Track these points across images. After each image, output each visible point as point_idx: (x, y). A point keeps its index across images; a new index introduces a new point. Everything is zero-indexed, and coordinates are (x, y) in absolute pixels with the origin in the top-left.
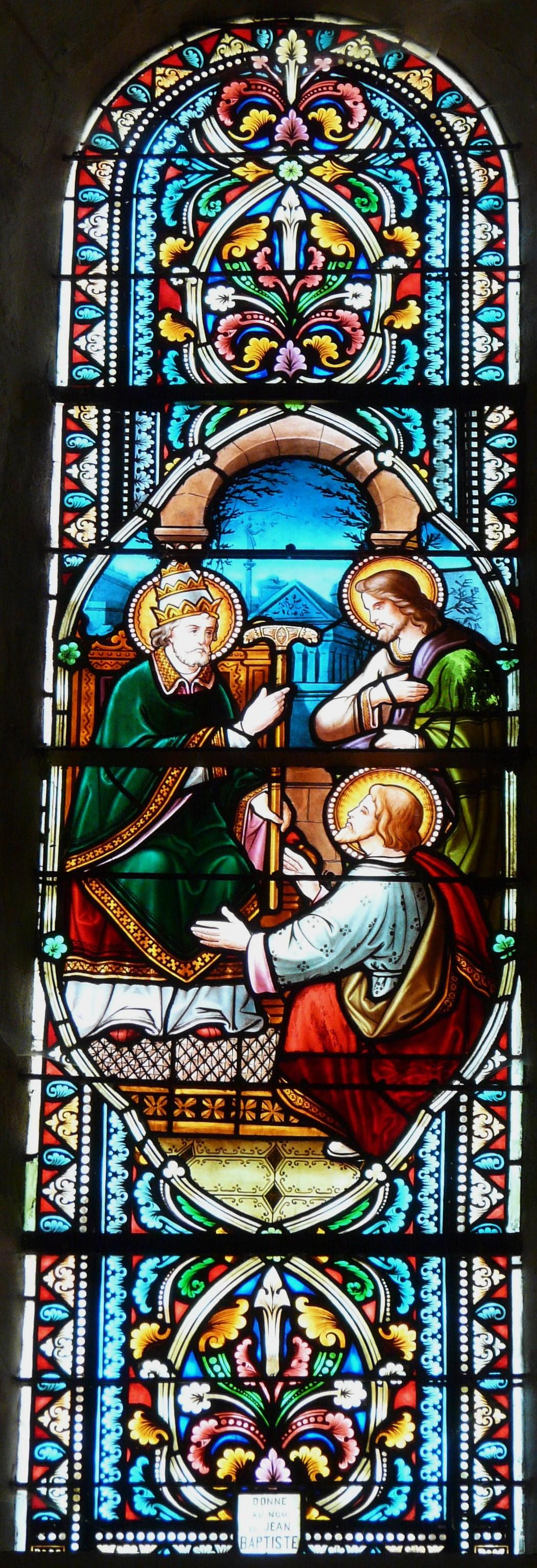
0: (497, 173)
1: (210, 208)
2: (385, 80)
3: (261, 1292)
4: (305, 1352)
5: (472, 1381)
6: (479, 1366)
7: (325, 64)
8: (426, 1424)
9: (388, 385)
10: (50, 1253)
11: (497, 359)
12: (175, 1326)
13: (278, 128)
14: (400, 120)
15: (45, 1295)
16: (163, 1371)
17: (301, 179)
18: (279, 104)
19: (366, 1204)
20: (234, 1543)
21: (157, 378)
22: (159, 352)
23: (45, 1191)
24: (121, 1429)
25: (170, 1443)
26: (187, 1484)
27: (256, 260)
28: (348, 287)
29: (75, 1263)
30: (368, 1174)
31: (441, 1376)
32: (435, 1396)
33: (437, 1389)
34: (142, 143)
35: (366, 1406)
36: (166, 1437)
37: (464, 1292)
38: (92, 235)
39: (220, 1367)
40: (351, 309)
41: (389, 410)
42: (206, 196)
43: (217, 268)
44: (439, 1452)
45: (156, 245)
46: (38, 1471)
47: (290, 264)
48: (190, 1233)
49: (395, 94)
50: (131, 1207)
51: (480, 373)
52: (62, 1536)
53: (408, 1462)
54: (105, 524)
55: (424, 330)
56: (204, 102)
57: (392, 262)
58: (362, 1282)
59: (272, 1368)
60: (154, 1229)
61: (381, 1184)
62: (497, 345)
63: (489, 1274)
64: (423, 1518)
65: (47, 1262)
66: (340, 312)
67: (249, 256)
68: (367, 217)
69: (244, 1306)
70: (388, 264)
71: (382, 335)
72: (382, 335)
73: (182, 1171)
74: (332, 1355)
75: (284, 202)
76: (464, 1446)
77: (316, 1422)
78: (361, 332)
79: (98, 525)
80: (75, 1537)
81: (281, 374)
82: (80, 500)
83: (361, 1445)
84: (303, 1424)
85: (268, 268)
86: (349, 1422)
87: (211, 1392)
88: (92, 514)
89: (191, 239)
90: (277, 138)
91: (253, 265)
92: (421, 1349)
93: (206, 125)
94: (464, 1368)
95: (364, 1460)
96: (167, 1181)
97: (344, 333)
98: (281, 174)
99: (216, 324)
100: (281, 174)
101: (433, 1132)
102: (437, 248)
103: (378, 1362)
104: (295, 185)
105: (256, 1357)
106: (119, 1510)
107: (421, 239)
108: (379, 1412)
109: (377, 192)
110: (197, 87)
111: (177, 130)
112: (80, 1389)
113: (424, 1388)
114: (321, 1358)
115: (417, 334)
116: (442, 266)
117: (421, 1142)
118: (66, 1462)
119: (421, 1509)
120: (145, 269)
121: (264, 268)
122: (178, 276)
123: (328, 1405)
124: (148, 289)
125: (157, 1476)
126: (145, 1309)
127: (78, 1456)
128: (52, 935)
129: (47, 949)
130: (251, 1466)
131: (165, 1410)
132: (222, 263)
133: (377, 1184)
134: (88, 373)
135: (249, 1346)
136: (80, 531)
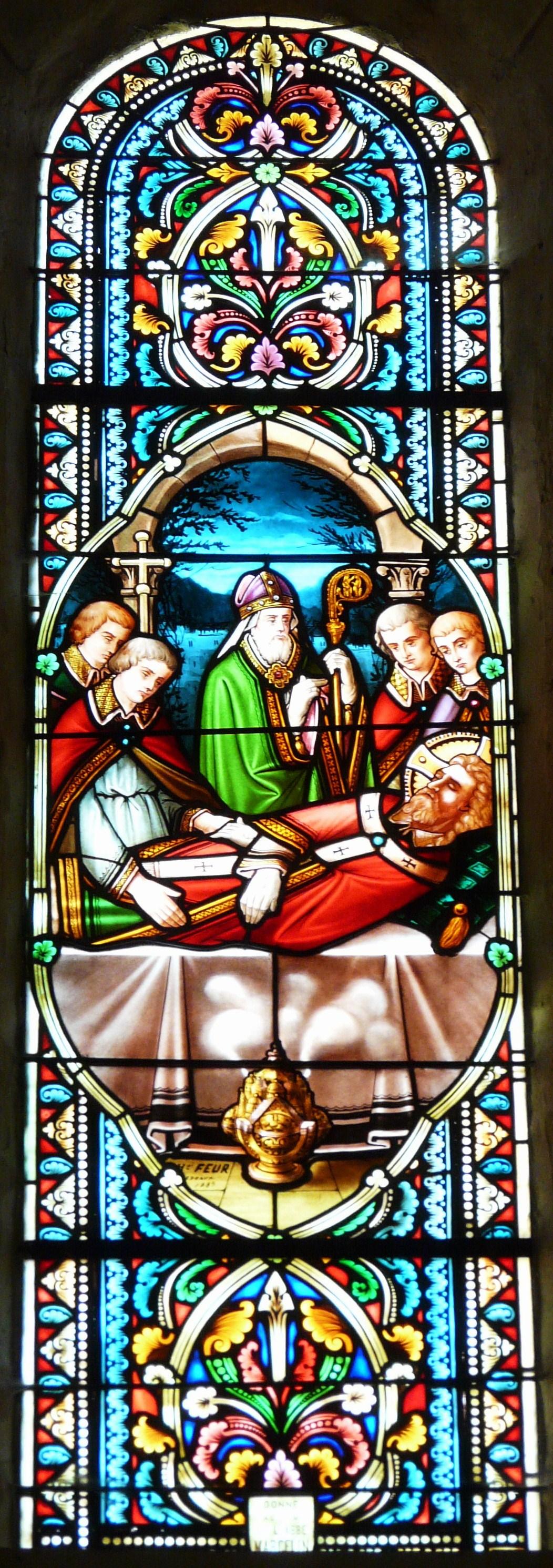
0: (475, 177)
1: (190, 1290)
3: (257, 210)
4: (310, 1355)
9: (370, 390)
11: (480, 363)
12: (178, 1329)
17: (279, 181)
19: (370, 1210)
23: (44, 1202)
24: (128, 250)
25: (176, 1450)
26: (195, 1489)
27: (232, 260)
30: (369, 1181)
31: (424, 272)
32: (445, 1396)
33: (420, 284)
34: (113, 146)
35: (375, 1411)
36: (172, 1443)
39: (226, 1370)
40: (349, 1415)
41: (384, 1262)
43: (193, 266)
46: (43, 1476)
47: (268, 265)
48: (187, 386)
49: (371, 98)
53: (420, 1466)
54: (85, 525)
56: (177, 105)
57: (371, 266)
58: (364, 1281)
59: (279, 1373)
61: (384, 1190)
62: (479, 349)
67: (227, 254)
69: (241, 220)
73: (179, 1180)
74: (339, 1360)
75: (262, 201)
76: (476, 1450)
77: (324, 1426)
78: (344, 338)
79: (79, 528)
81: (261, 374)
85: (246, 269)
87: (217, 1397)
88: (72, 516)
89: (169, 231)
90: (253, 142)
91: (230, 265)
92: (428, 1349)
93: (179, 127)
96: (165, 1190)
97: (320, 108)
98: (258, 178)
99: (197, 1434)
100: (258, 178)
101: (437, 1133)
104: (272, 186)
106: (127, 1513)
108: (389, 1416)
109: (375, 1277)
110: (170, 92)
112: (83, 1494)
113: (433, 1390)
114: (328, 1362)
115: (400, 340)
116: (451, 1486)
117: (426, 1145)
118: (79, 319)
121: (241, 268)
122: (155, 271)
123: (336, 1410)
124: (124, 309)
126: (146, 1313)
128: (45, 651)
129: (39, 666)
131: (171, 1417)
132: (199, 259)
133: (379, 1190)
134: (63, 370)
135: (244, 254)
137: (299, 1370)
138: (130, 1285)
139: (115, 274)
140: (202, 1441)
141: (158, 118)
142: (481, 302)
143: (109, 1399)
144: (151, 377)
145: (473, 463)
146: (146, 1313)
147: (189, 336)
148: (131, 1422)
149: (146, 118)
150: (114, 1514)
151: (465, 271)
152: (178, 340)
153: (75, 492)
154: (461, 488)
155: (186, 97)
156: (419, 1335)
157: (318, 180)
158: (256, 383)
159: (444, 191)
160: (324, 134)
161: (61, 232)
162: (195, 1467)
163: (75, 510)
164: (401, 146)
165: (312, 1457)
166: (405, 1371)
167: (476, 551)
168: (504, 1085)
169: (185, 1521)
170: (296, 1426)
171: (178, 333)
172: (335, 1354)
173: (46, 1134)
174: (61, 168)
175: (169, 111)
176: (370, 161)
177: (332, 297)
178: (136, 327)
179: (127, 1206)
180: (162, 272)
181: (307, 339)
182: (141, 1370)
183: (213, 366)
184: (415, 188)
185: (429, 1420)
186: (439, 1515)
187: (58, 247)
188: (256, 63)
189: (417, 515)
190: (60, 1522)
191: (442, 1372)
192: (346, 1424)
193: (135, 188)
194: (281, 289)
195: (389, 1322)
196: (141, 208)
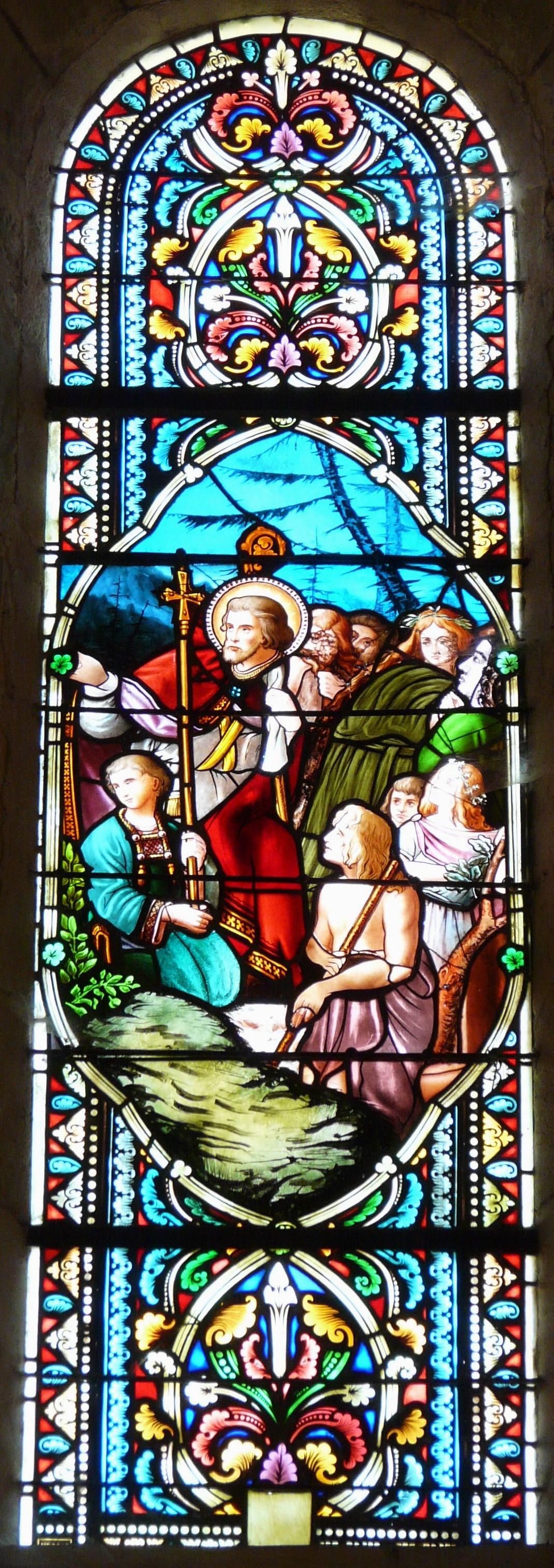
3: (274, 216)
4: (313, 1349)
11: (496, 368)
14: (392, 132)
15: (47, 1356)
18: (273, 114)
20: (243, 1537)
26: (199, 1486)
27: (251, 266)
28: (341, 292)
35: (368, 311)
37: (476, 1429)
40: (345, 314)
42: (200, 206)
45: (130, 1322)
50: (137, 1205)
51: (478, 267)
52: (70, 1529)
53: (419, 1459)
55: (421, 261)
58: (361, 206)
60: (154, 1510)
61: (392, 1176)
63: (501, 1411)
66: (335, 319)
67: (246, 260)
68: (364, 227)
69: (259, 225)
70: (383, 274)
71: (380, 341)
72: (380, 341)
80: (82, 1529)
81: (276, 371)
82: (81, 322)
86: (352, 323)
89: (186, 240)
91: (249, 271)
93: (196, 135)
99: (198, 1420)
102: (432, 255)
104: (289, 195)
105: (262, 1352)
106: (126, 1504)
107: (417, 247)
109: (379, 1272)
110: (188, 99)
117: (429, 1142)
119: (434, 1508)
122: (173, 278)
123: (333, 310)
125: (165, 1478)
126: (165, 223)
132: (218, 265)
136: (81, 295)
139: (130, 280)
140: (203, 1428)
141: (176, 127)
142: (512, 1151)
143: (112, 1391)
144: (154, 1206)
146: (165, 223)
147: (203, 340)
148: (147, 313)
149: (164, 126)
150: (113, 1503)
151: (484, 280)
152: (193, 345)
153: (96, 257)
155: (203, 105)
156: (412, 243)
158: (269, 381)
159: (461, 204)
161: (75, 304)
162: (208, 128)
165: (312, 344)
168: (499, 434)
169: (183, 1512)
171: (193, 338)
174: (78, 179)
177: (348, 301)
178: (152, 331)
179: (127, 1475)
180: (179, 278)
181: (325, 1448)
183: (227, 368)
189: (434, 522)
190: (58, 1509)
191: (434, 274)
193: (153, 196)
194: (299, 293)
195: (385, 231)
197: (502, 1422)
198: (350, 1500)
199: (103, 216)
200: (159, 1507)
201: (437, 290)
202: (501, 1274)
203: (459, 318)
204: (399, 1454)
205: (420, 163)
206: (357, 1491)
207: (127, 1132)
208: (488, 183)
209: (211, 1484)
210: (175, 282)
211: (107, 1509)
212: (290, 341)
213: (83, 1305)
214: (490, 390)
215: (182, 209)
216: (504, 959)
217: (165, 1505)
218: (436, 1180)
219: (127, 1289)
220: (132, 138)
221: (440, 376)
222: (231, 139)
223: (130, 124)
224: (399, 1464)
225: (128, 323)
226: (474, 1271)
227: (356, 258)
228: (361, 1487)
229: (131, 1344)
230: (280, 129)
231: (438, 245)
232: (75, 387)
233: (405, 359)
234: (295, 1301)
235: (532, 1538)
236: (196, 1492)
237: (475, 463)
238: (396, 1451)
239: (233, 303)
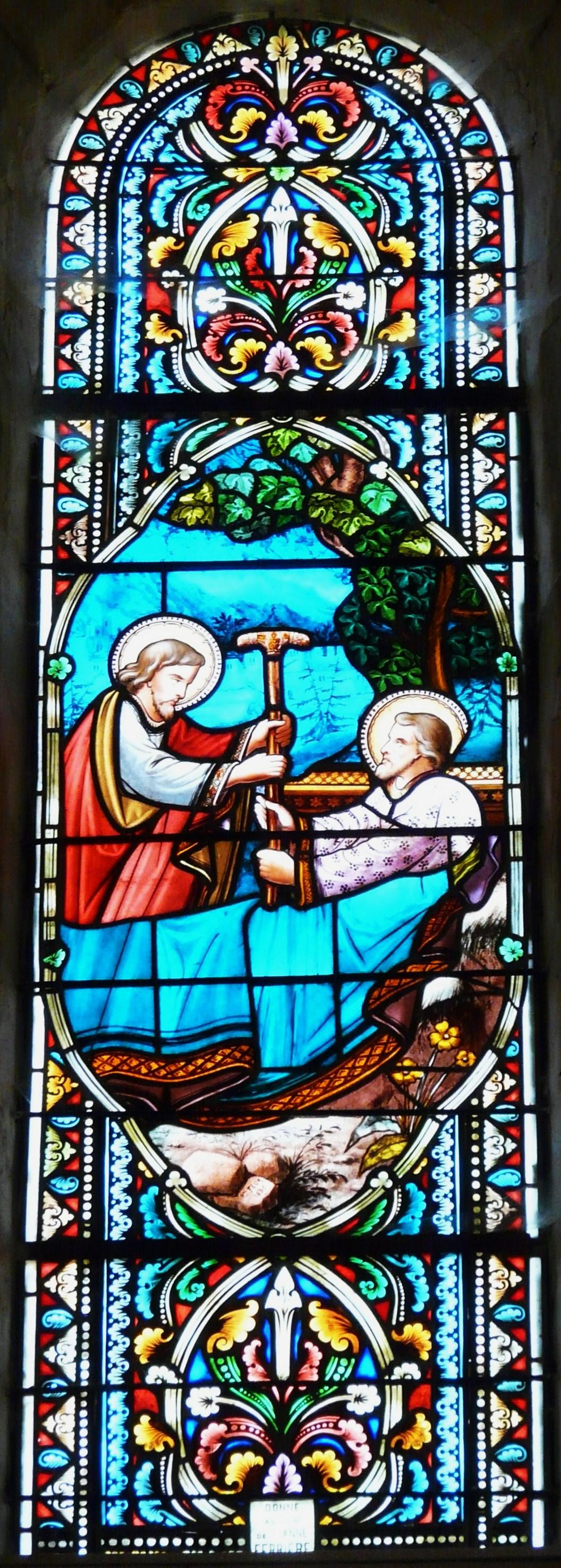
1: (190, 1291)
2: (393, 1543)
3: (270, 210)
5: (489, 1383)
6: (494, 1370)
7: (315, 63)
8: (442, 1424)
10: (50, 1260)
11: (496, 359)
13: (268, 359)
16: (171, 1377)
17: (293, 179)
21: (136, 1231)
22: (135, 1459)
25: (176, 1450)
26: (199, 1497)
29: (78, 1269)
32: (451, 1395)
35: (379, 1412)
36: (171, 1443)
38: (78, 243)
41: (392, 1260)
44: (456, 1452)
45: (143, 248)
56: (192, 102)
59: (283, 1370)
60: (155, 1522)
63: (506, 1276)
64: (440, 1520)
65: (47, 1269)
68: (364, 222)
69: (253, 1306)
70: (398, 1373)
75: (278, 1283)
81: (273, 147)
83: (374, 1451)
84: (316, 1428)
92: (436, 1348)
93: (194, 128)
94: (481, 1370)
95: (378, 1463)
103: (391, 1362)
104: (287, 185)
105: (266, 1359)
108: (394, 1414)
110: (184, 89)
111: (166, 130)
112: (84, 1503)
117: (435, 1141)
119: (438, 1511)
120: (134, 272)
122: (169, 280)
123: (340, 1411)
127: (84, 1462)
130: (262, 355)
131: (172, 1415)
137: (305, 1370)
138: (131, 1288)
141: (172, 116)
145: (490, 462)
147: (202, 333)
151: (485, 268)
152: (192, 350)
154: (478, 489)
155: (200, 94)
157: (331, 179)
158: (267, 386)
160: (340, 361)
162: (195, 1468)
163: (89, 331)
164: (420, 141)
166: (411, 1370)
167: (490, 557)
170: (298, 1426)
172: (340, 1355)
173: (49, 1289)
175: (182, 108)
176: (388, 160)
177: (346, 296)
180: (177, 280)
182: (143, 1370)
183: (222, 137)
184: (432, 185)
185: (434, 1418)
186: (443, 1515)
187: (70, 260)
188: (272, 57)
189: (433, 518)
191: (452, 1371)
192: (352, 1428)
193: (147, 194)
196: (155, 218)
197: (484, 233)
198: (352, 1507)
199: (97, 211)
200: (160, 1519)
201: (434, 282)
202: (508, 1415)
203: (457, 230)
204: (404, 1460)
205: (421, 148)
206: (361, 1499)
207: (123, 1138)
208: (488, 167)
209: (211, 1495)
210: (172, 284)
211: (107, 1522)
212: (286, 117)
213: (79, 1458)
214: (488, 380)
215: (176, 210)
216: (499, 661)
217: (165, 1518)
218: (427, 433)
219: (124, 1412)
220: (127, 129)
221: (455, 1359)
222: (227, 363)
223: (126, 114)
224: (403, 1471)
225: (112, 1299)
226: (460, 293)
227: (354, 251)
228: (364, 1494)
229: (129, 1354)
230: (276, 118)
231: (437, 354)
232: (69, 390)
233: (415, 1478)
234: (299, 1305)
235: (538, 1540)
236: (196, 1502)
237: (477, 454)
238: (400, 1458)
239: (230, 305)
